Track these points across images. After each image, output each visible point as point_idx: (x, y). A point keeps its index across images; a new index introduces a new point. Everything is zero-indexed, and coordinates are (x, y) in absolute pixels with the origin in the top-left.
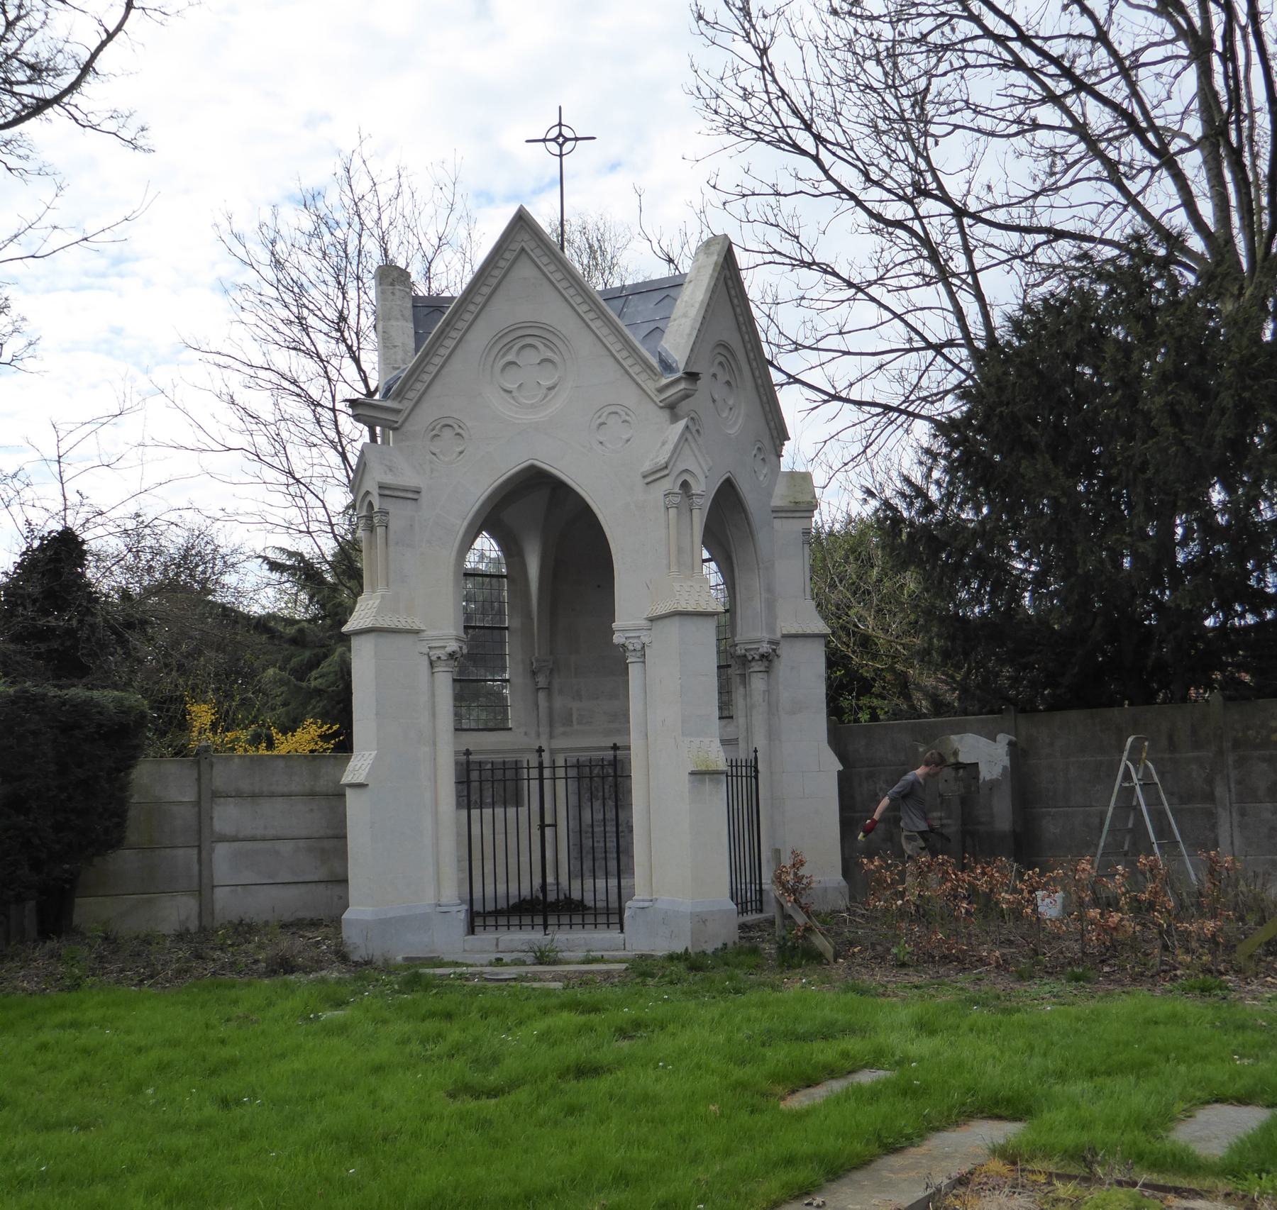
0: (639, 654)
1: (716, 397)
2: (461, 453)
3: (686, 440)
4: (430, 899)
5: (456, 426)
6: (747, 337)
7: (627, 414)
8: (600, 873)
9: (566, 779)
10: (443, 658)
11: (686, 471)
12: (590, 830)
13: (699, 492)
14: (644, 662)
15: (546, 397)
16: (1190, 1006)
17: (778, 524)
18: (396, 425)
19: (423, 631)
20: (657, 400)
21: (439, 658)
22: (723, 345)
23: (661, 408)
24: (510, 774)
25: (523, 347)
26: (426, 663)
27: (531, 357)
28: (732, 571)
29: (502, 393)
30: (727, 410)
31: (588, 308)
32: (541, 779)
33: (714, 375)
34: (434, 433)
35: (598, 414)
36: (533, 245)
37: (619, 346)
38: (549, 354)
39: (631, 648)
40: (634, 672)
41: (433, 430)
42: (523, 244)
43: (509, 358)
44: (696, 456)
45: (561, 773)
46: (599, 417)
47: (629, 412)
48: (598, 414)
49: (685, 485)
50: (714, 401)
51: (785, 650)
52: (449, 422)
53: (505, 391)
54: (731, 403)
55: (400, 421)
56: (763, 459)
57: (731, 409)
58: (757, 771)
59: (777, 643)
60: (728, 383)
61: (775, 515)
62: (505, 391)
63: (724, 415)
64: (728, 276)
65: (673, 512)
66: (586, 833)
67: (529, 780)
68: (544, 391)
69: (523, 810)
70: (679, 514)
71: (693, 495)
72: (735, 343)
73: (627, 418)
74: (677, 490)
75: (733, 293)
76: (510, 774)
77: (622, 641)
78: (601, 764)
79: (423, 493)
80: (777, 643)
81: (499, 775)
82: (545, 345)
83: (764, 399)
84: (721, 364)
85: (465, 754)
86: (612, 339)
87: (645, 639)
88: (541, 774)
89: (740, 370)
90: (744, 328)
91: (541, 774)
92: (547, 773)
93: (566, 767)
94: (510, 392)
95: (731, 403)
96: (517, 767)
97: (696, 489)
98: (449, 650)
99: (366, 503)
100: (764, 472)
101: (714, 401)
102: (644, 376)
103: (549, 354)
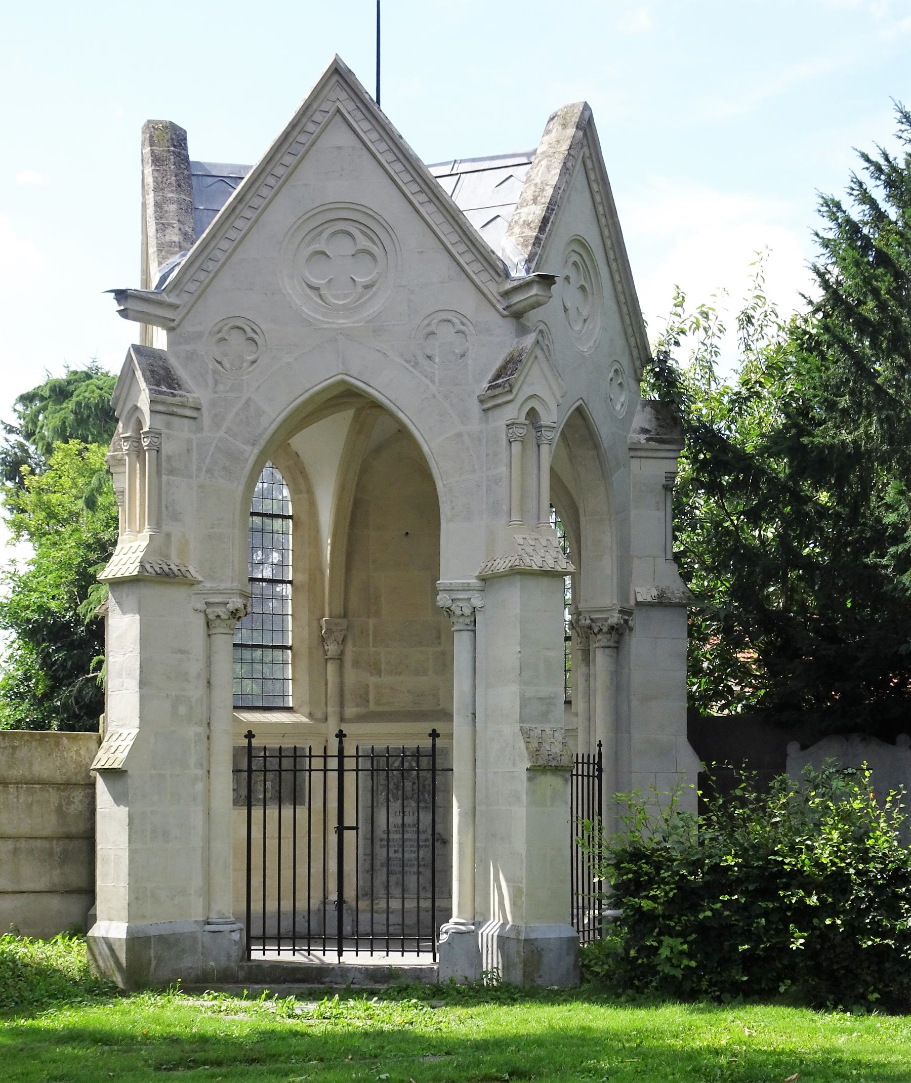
0: (468, 621)
1: (568, 305)
2: (254, 362)
3: (536, 357)
4: (198, 914)
5: (248, 329)
6: (606, 232)
7: (463, 324)
8: (396, 891)
9: (357, 771)
10: (224, 616)
11: (534, 396)
12: (385, 836)
13: (549, 423)
14: (474, 631)
15: (360, 298)
16: (234, 1017)
17: (635, 463)
18: (172, 324)
19: (199, 582)
20: (500, 307)
21: (218, 616)
22: (580, 241)
23: (504, 317)
24: (287, 763)
25: (335, 233)
26: (202, 622)
27: (343, 247)
28: (578, 522)
29: (307, 289)
30: (581, 322)
31: (419, 189)
32: (341, 771)
33: (567, 278)
34: (220, 335)
35: (429, 319)
36: (351, 106)
37: (455, 238)
38: (367, 244)
39: (458, 612)
40: (461, 644)
41: (219, 332)
42: (338, 104)
43: (317, 247)
44: (546, 379)
45: (349, 764)
46: (429, 325)
47: (465, 321)
48: (426, 322)
49: (532, 414)
50: (566, 310)
51: (636, 622)
52: (239, 323)
53: (310, 287)
54: (585, 313)
55: (177, 320)
56: (620, 384)
57: (585, 321)
58: (600, 770)
59: (630, 613)
60: (582, 288)
61: (632, 454)
62: (310, 287)
63: (577, 328)
64: (587, 154)
65: (516, 447)
66: (426, 840)
67: (310, 771)
68: (360, 289)
69: (302, 811)
70: (523, 449)
71: (541, 427)
72: (594, 241)
73: (463, 328)
74: (522, 419)
75: (592, 176)
76: (287, 763)
77: (449, 603)
78: (417, 754)
79: (204, 411)
80: (630, 613)
81: (273, 763)
82: (362, 232)
83: (625, 310)
84: (575, 264)
85: (246, 737)
86: (446, 228)
87: (477, 602)
88: (341, 764)
89: (597, 273)
90: (603, 221)
91: (341, 764)
92: (333, 763)
93: (357, 757)
94: (317, 289)
95: (585, 313)
96: (296, 754)
97: (546, 419)
98: (231, 607)
99: (133, 420)
100: (622, 399)
101: (566, 310)
102: (485, 277)
103: (367, 244)
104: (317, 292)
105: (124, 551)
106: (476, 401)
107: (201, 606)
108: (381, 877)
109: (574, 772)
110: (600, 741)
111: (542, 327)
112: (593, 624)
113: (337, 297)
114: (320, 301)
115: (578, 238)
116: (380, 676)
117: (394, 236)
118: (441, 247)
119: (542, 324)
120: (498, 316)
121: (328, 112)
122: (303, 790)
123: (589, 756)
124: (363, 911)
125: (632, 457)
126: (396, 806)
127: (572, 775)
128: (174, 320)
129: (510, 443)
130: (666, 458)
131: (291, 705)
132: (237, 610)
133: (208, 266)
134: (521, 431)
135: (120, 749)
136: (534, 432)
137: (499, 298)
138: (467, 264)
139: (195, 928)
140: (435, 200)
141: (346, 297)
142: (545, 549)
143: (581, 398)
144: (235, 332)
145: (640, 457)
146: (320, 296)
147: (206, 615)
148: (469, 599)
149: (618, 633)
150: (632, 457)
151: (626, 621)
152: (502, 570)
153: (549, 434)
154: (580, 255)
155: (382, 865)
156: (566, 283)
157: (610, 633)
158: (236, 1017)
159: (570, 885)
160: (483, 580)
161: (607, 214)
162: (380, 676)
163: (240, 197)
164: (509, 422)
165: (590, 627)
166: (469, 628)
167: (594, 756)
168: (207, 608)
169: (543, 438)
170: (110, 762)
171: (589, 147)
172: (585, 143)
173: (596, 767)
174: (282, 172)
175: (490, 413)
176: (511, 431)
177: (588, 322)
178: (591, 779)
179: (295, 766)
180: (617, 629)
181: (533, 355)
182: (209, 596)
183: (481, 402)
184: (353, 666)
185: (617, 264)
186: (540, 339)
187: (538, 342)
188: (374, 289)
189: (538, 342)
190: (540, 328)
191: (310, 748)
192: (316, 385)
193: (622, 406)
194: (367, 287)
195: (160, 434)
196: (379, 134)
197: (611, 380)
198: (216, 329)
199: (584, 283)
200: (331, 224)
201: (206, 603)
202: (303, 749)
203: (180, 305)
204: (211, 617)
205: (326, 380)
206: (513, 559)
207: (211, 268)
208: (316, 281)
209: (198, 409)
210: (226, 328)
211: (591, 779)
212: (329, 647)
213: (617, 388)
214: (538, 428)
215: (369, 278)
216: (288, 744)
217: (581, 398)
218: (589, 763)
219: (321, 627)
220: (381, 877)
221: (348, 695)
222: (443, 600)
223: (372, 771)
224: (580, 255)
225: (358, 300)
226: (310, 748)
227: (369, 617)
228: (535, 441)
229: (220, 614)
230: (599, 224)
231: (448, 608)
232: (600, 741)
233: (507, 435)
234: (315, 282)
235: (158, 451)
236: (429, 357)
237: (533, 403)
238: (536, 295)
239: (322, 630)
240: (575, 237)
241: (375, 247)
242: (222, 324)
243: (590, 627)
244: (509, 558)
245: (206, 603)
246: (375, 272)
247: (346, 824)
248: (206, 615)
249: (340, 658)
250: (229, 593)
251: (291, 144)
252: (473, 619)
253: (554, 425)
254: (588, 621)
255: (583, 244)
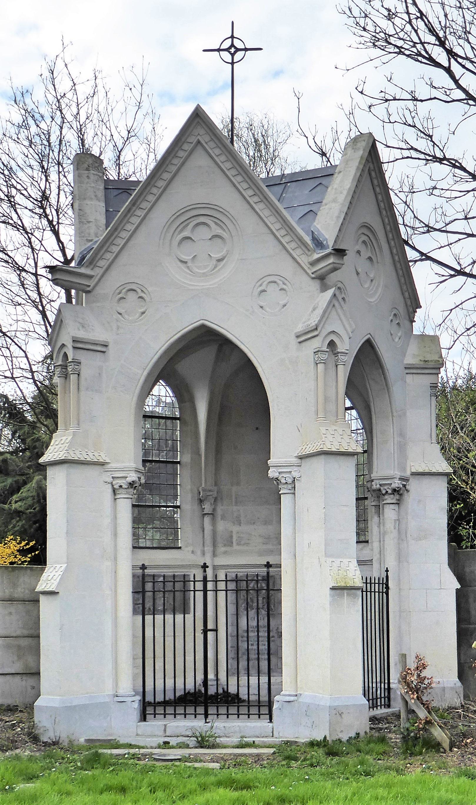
0: (290, 487)
1: (360, 270)
2: (143, 313)
3: (334, 306)
10: (124, 486)
11: (333, 332)
12: (246, 634)
14: (294, 494)
15: (215, 267)
17: (409, 378)
20: (310, 272)
21: (121, 486)
22: (366, 226)
27: (203, 233)
29: (179, 263)
32: (205, 591)
33: (359, 252)
34: (120, 296)
37: (278, 226)
39: (283, 481)
41: (119, 293)
42: (199, 137)
43: (186, 233)
46: (261, 285)
47: (286, 282)
49: (332, 344)
50: (358, 274)
51: (413, 485)
53: (182, 261)
54: (372, 276)
56: (398, 324)
57: (372, 281)
58: (387, 588)
59: (407, 480)
60: (370, 259)
62: (182, 261)
65: (321, 367)
66: (242, 637)
67: (194, 591)
68: (214, 262)
69: (189, 617)
70: (326, 369)
71: (338, 353)
73: (284, 287)
74: (325, 348)
75: (375, 182)
76: (179, 586)
77: (276, 475)
80: (407, 480)
82: (216, 223)
83: (400, 272)
84: (364, 242)
85: (141, 568)
87: (295, 474)
88: (205, 586)
89: (380, 248)
91: (205, 586)
92: (210, 586)
94: (186, 263)
96: (185, 580)
97: (341, 347)
98: (129, 480)
100: (399, 334)
101: (358, 274)
103: (219, 231)
104: (185, 265)
105: (57, 443)
106: (293, 337)
107: (110, 480)
108: (243, 663)
109: (365, 590)
110: (387, 568)
111: (340, 285)
112: (382, 488)
113: (199, 268)
114: (188, 271)
115: (366, 225)
116: (240, 525)
117: (238, 227)
118: (269, 232)
119: (340, 283)
120: (309, 279)
121: (192, 143)
122: (189, 603)
123: (366, 578)
124: (244, 686)
125: (407, 374)
126: (252, 613)
127: (362, 591)
128: (89, 286)
129: (317, 364)
130: (430, 374)
131: (180, 546)
132: (133, 482)
133: (112, 249)
134: (324, 356)
135: (55, 578)
136: (333, 356)
137: (309, 266)
138: (287, 243)
139: (107, 700)
140: (264, 200)
141: (205, 267)
142: (342, 437)
143: (370, 334)
144: (131, 294)
145: (413, 373)
146: (188, 268)
147: (113, 486)
148: (291, 472)
149: (398, 494)
150: (407, 374)
151: (404, 486)
152: (312, 452)
153: (343, 358)
154: (368, 236)
155: (244, 654)
156: (358, 255)
157: (393, 494)
158: (125, 761)
159: (173, 673)
160: (300, 458)
161: (387, 208)
162: (240, 525)
163: (133, 201)
164: (315, 350)
165: (380, 490)
166: (292, 492)
167: (383, 578)
168: (113, 480)
169: (339, 361)
170: (51, 587)
171: (373, 163)
172: (370, 160)
173: (384, 586)
174: (162, 184)
175: (304, 344)
176: (317, 356)
177: (374, 281)
178: (381, 594)
179: (216, 588)
180: (398, 491)
181: (332, 305)
182: (113, 473)
183: (298, 337)
184: (222, 519)
185: (395, 242)
186: (337, 293)
187: (335, 295)
188: (224, 261)
189: (335, 295)
190: (338, 286)
191: (194, 575)
192: (185, 328)
193: (400, 338)
194: (219, 260)
195: (80, 363)
196: (227, 156)
197: (392, 321)
198: (118, 291)
199: (371, 255)
200: (194, 218)
201: (113, 478)
202: (188, 575)
203: (94, 276)
204: (116, 487)
205: (192, 324)
206: (319, 444)
207: (114, 250)
208: (184, 257)
209: (106, 346)
210: (124, 290)
211: (381, 594)
212: (205, 506)
213: (396, 327)
214: (336, 354)
215: (220, 255)
216: (179, 572)
217: (370, 334)
218: (371, 583)
219: (200, 492)
220: (243, 663)
221: (219, 539)
222: (272, 473)
223: (237, 591)
224: (368, 236)
225: (213, 270)
226: (194, 575)
227: (232, 486)
228: (334, 363)
229: (122, 484)
230: (381, 215)
231: (277, 478)
232: (387, 568)
233: (314, 359)
234: (184, 258)
235: (79, 375)
236: (262, 307)
237: (333, 337)
238: (333, 263)
239: (200, 494)
240: (363, 224)
241: (224, 233)
242: (120, 288)
243: (380, 490)
244: (313, 444)
245: (113, 478)
246: (225, 250)
247: (209, 628)
248: (113, 486)
249: (213, 515)
250: (127, 471)
251: (167, 165)
252: (293, 486)
253: (347, 352)
254: (378, 486)
255: (370, 228)
